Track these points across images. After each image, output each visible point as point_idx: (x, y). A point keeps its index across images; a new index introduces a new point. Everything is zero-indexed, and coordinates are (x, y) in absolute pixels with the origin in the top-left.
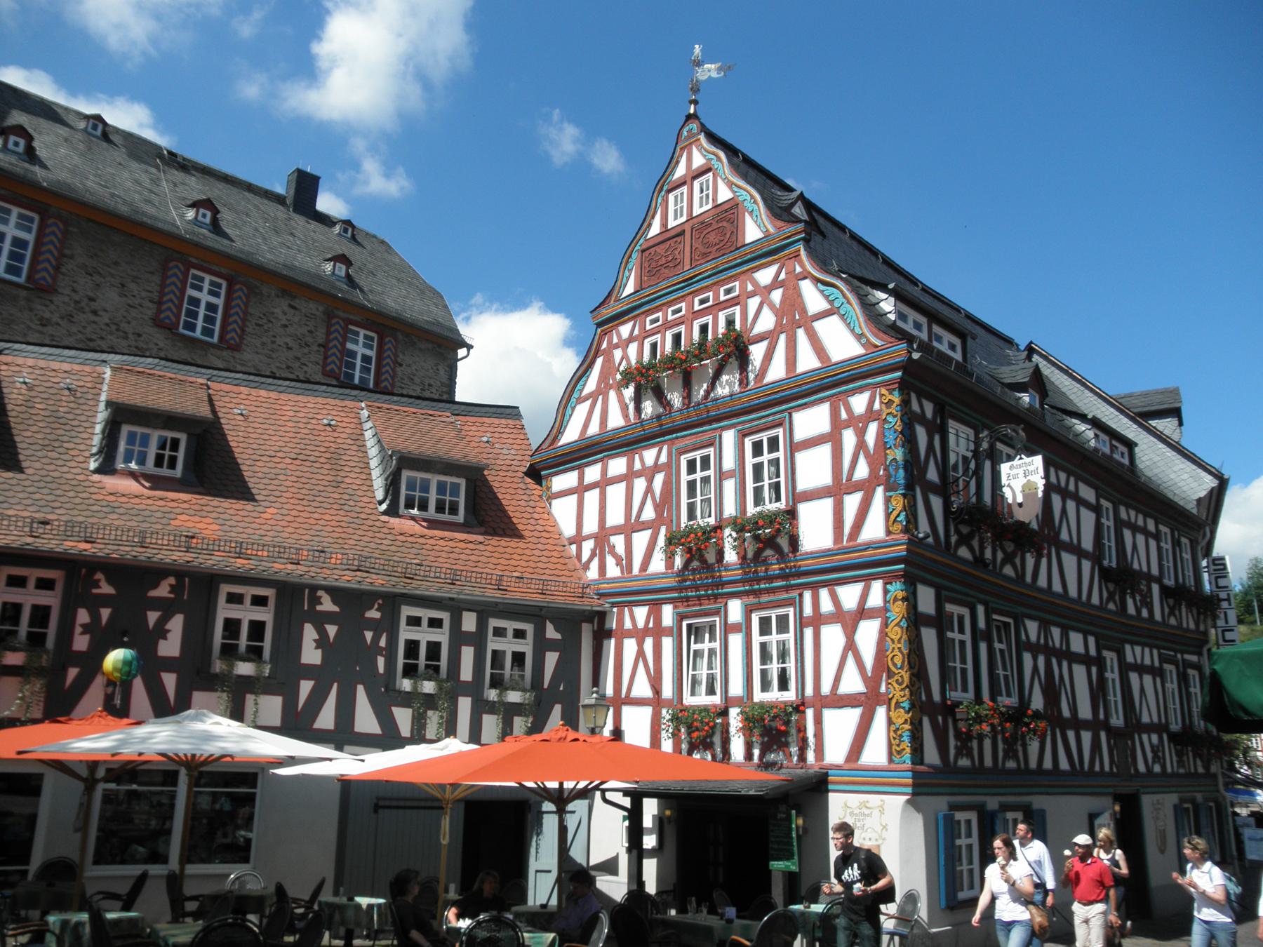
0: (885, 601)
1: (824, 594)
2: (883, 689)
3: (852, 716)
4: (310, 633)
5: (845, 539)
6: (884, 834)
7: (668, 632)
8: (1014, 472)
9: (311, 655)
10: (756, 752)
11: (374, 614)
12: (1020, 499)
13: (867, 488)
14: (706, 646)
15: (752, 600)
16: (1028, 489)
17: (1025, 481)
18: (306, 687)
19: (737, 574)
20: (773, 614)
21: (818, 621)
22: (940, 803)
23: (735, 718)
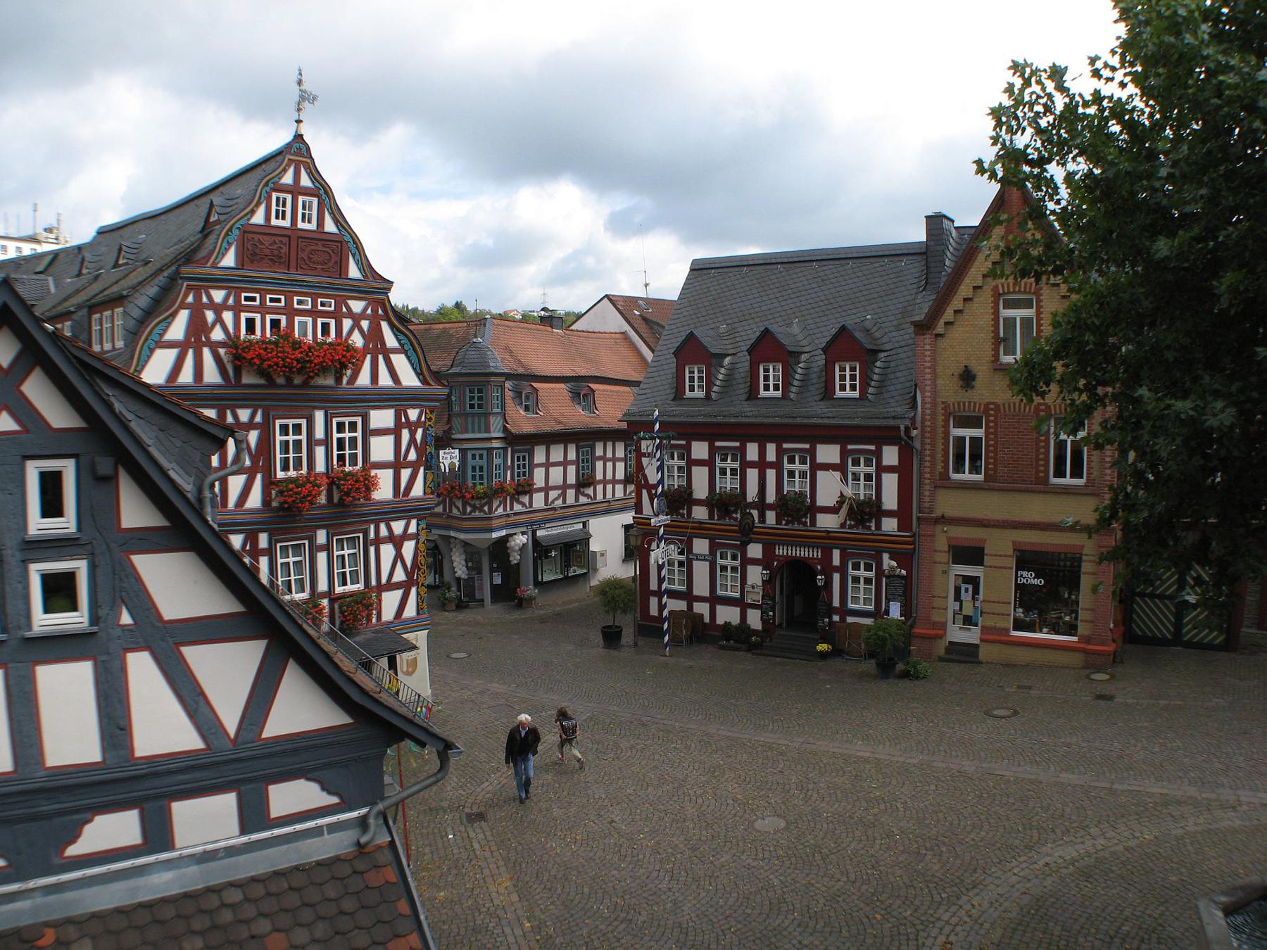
2: (415, 577)
3: (398, 593)
7: (771, 465)
13: (415, 466)
21: (378, 542)
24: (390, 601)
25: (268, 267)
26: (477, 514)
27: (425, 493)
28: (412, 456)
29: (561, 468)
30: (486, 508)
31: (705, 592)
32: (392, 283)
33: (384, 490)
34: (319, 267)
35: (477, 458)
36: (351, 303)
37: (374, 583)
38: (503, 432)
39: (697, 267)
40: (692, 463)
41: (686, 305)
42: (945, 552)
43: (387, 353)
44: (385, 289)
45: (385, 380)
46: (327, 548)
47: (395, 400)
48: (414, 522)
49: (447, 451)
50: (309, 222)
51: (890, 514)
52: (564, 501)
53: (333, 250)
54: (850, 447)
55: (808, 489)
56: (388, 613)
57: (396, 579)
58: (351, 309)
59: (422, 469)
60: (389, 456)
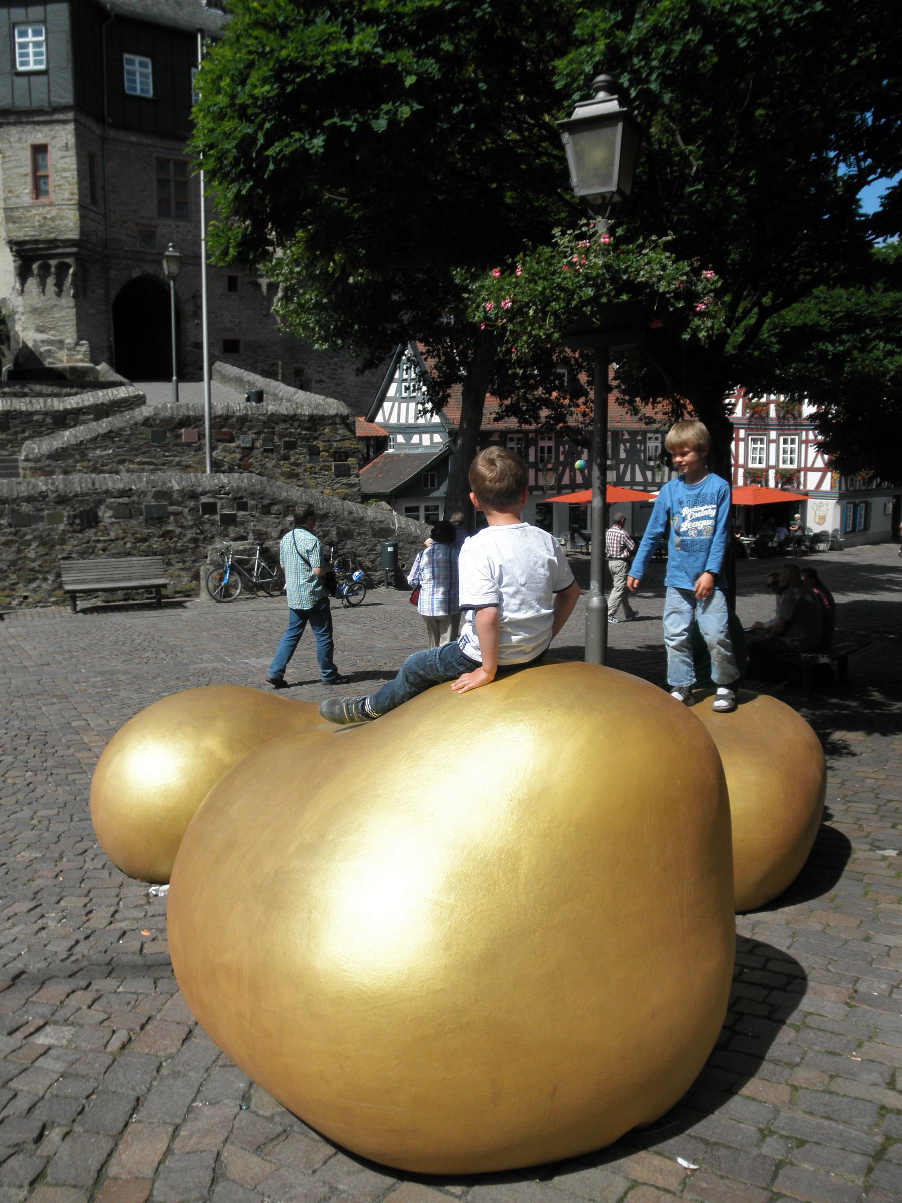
3: (819, 475)
4: (622, 447)
9: (623, 455)
10: (780, 485)
11: (640, 438)
14: (759, 446)
15: (780, 432)
18: (622, 466)
19: (775, 422)
20: (789, 438)
22: (844, 502)
23: (772, 473)
46: (776, 441)
56: (811, 485)
57: (817, 465)
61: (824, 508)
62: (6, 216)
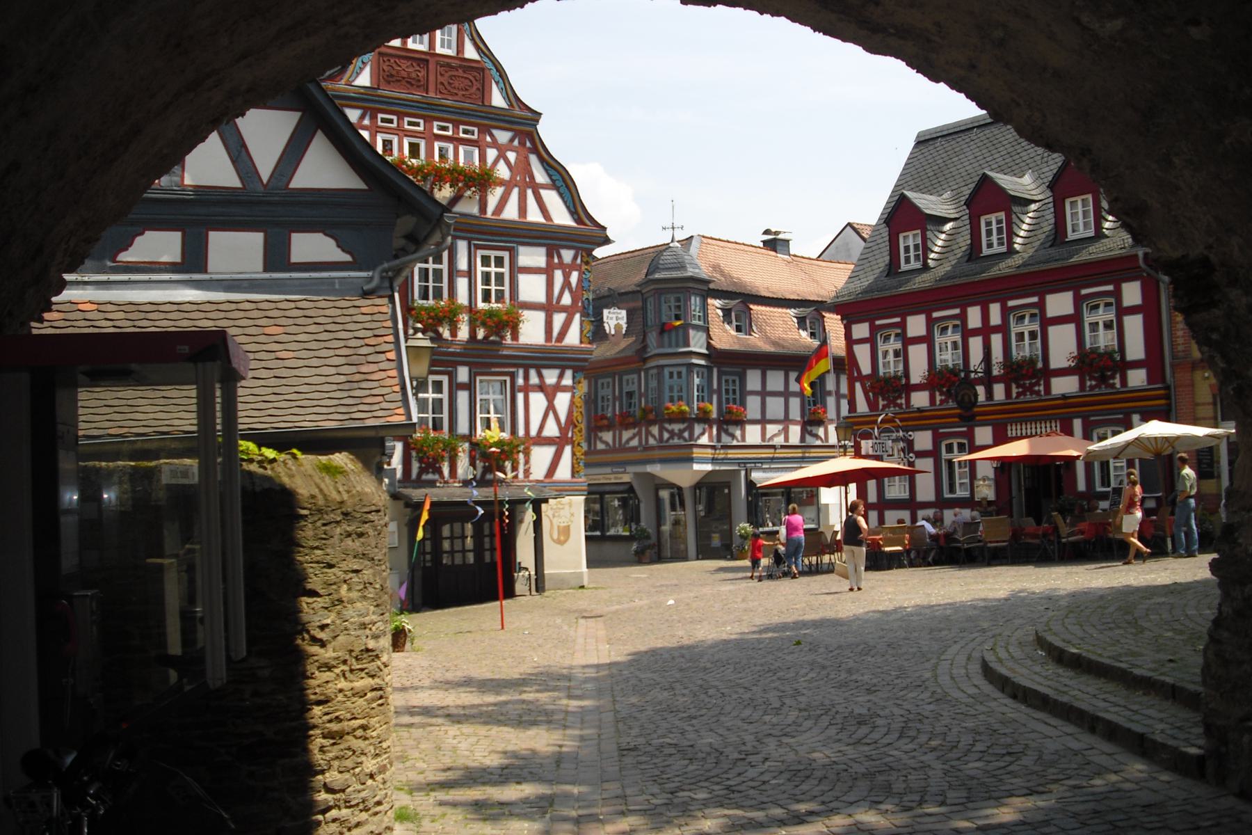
0: (574, 383)
1: (533, 373)
2: (570, 435)
3: (549, 452)
5: (554, 340)
6: (572, 519)
7: (996, 329)
8: (611, 316)
12: (613, 332)
13: (569, 311)
16: (618, 327)
17: (616, 322)
21: (526, 389)
24: (541, 457)
25: (404, 89)
26: (676, 441)
27: (581, 342)
28: (567, 300)
29: (782, 399)
30: (686, 434)
31: (931, 497)
32: (540, 114)
33: (532, 331)
34: (461, 93)
35: (675, 376)
36: (496, 132)
37: (521, 432)
38: (707, 349)
39: (923, 139)
40: (908, 342)
41: (908, 179)
42: (1209, 404)
43: (536, 188)
44: (532, 120)
45: (534, 216)
47: (547, 238)
48: (569, 373)
49: (612, 310)
50: (449, 47)
51: (1136, 365)
52: (786, 439)
53: (474, 77)
54: (1084, 292)
55: (1040, 352)
58: (496, 140)
59: (577, 316)
60: (541, 298)
61: (565, 512)
62: (705, 553)
